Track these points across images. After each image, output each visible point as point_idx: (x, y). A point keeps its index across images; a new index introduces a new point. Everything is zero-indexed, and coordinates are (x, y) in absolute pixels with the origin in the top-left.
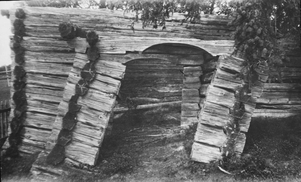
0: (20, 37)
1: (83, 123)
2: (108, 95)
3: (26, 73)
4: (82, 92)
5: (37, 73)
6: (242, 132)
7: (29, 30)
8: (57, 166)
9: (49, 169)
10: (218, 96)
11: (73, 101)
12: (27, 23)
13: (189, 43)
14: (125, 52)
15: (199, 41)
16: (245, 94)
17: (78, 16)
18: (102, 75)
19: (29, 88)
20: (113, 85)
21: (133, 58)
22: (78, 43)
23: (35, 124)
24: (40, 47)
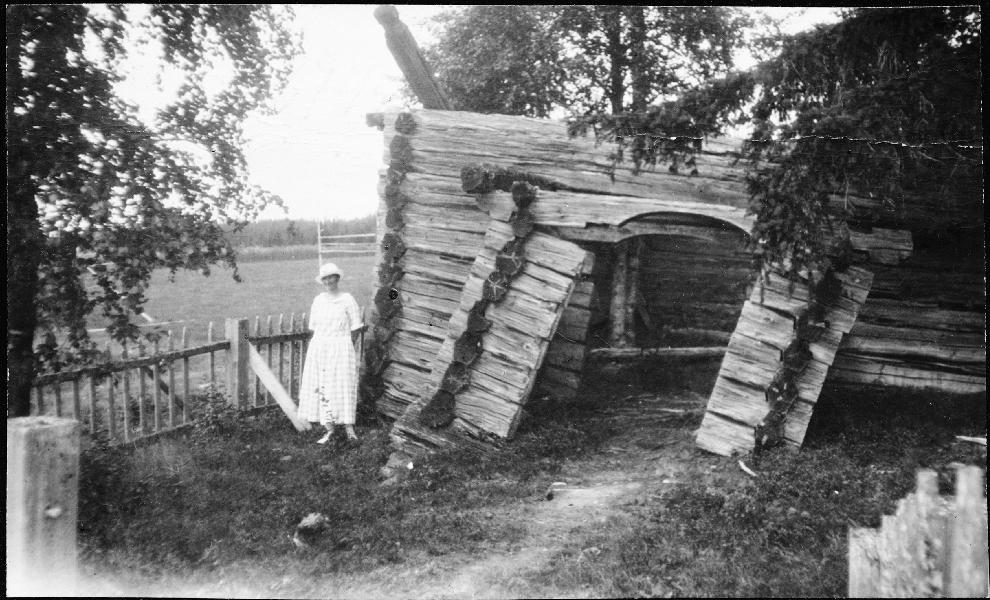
0: (400, 174)
1: (493, 355)
2: (545, 305)
3: (406, 249)
4: (496, 295)
5: (429, 252)
6: (806, 401)
7: (422, 160)
8: (436, 429)
9: (423, 434)
10: (758, 323)
11: (478, 313)
12: (418, 145)
13: (711, 214)
14: (584, 225)
15: (733, 211)
16: (811, 323)
17: (524, 133)
18: (539, 265)
19: (410, 282)
20: (557, 286)
21: (637, 233)
22: (495, 201)
23: (416, 359)
24: (439, 197)
